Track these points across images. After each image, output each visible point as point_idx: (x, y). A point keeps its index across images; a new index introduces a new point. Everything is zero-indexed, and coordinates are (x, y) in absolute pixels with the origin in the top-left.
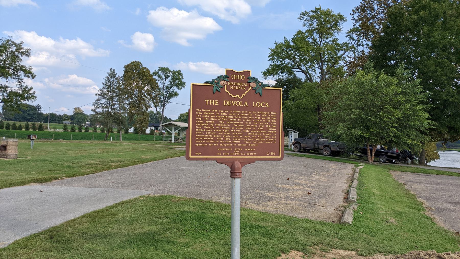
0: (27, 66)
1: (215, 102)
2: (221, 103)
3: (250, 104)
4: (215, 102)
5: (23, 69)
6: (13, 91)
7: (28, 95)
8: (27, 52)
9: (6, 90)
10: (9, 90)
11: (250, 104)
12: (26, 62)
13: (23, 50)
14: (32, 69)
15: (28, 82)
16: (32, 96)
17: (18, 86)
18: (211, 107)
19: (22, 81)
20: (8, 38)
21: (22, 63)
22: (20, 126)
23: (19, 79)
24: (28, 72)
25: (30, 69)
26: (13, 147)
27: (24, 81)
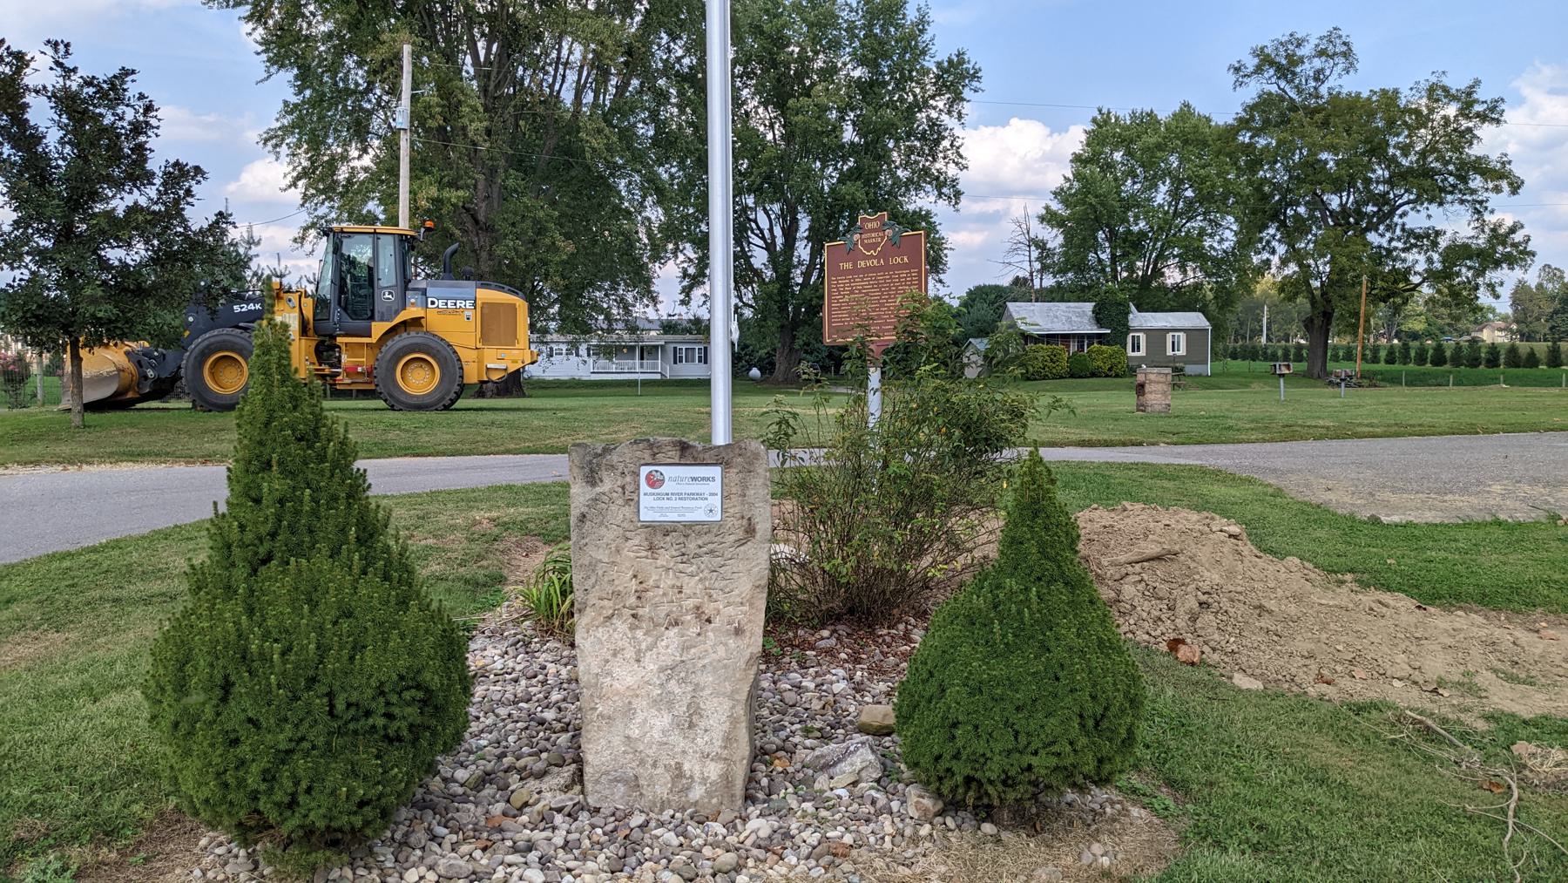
0: (1494, 156)
1: (848, 266)
2: (855, 265)
3: (886, 261)
4: (848, 266)
5: (1480, 167)
6: (1459, 242)
7: (1508, 249)
8: (1493, 109)
9: (1435, 244)
10: (1443, 243)
11: (886, 261)
12: (1488, 142)
13: (1478, 108)
14: (1510, 162)
15: (1503, 210)
16: (1521, 252)
17: (1472, 225)
18: (846, 272)
19: (1486, 208)
20: (1434, 79)
21: (1476, 151)
22: (1532, 354)
23: (1475, 201)
24: (1500, 175)
25: (1503, 163)
26: (1160, 387)
27: (1490, 205)
